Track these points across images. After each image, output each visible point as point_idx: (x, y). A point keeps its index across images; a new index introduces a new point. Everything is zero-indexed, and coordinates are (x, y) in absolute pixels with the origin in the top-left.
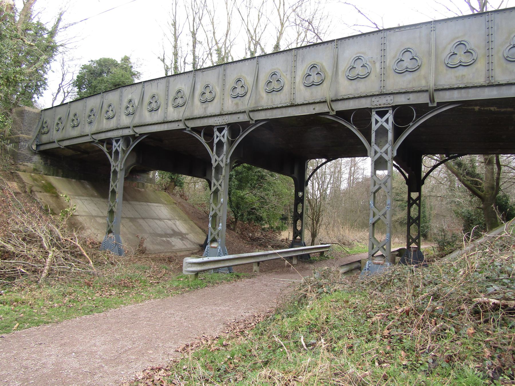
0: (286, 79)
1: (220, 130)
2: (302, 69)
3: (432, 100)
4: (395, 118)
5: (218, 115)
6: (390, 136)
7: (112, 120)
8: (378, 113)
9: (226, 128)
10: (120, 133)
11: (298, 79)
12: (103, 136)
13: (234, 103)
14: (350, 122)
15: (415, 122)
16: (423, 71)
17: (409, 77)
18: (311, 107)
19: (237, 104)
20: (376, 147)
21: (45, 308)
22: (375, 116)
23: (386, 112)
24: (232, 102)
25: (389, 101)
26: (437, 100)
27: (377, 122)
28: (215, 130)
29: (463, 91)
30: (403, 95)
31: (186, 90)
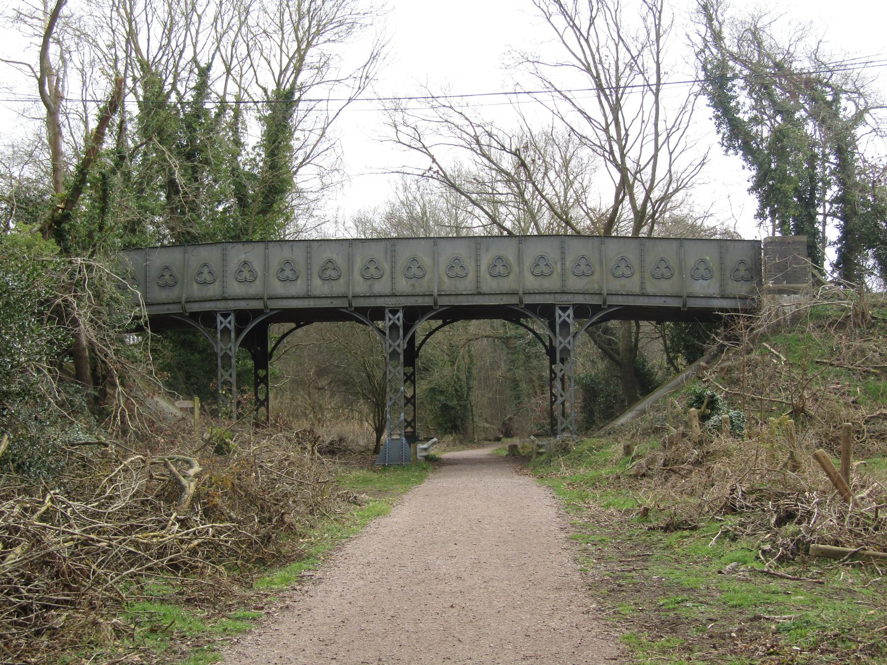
0: (471, 266)
1: (394, 312)
2: (486, 261)
3: (605, 302)
4: (404, 316)
5: (303, 298)
6: (233, 335)
7: (211, 286)
8: (222, 315)
9: (401, 311)
10: (232, 305)
11: (483, 268)
12: (195, 308)
13: (409, 283)
14: (536, 313)
15: (591, 318)
16: (596, 277)
17: (585, 280)
18: (499, 297)
19: (413, 285)
20: (560, 339)
21: (690, 642)
22: (220, 318)
23: (397, 311)
24: (407, 282)
25: (570, 299)
26: (439, 304)
27: (560, 316)
28: (387, 311)
29: (625, 297)
30: (581, 295)
31: (511, 257)
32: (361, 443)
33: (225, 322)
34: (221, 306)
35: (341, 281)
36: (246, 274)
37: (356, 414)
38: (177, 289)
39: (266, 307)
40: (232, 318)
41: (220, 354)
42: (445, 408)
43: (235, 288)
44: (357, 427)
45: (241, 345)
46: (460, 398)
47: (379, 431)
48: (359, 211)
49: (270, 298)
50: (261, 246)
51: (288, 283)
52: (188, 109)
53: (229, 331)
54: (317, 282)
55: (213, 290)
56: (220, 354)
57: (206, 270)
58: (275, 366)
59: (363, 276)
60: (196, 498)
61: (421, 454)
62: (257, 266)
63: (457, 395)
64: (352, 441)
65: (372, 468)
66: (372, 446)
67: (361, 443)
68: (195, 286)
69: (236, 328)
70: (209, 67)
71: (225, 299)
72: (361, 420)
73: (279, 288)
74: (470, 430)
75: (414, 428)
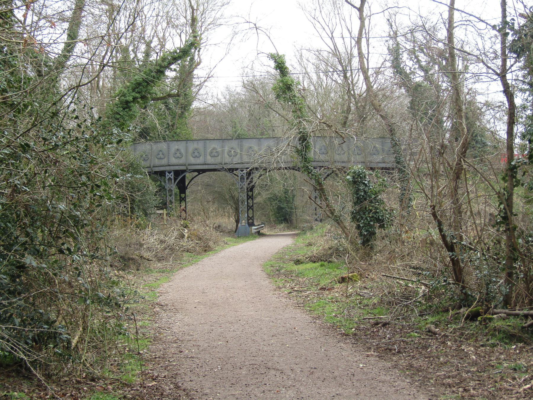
6: (173, 181)
12: (157, 169)
22: (167, 174)
32: (229, 228)
33: (170, 175)
34: (168, 168)
35: (219, 157)
36: (178, 155)
37: (227, 214)
38: (148, 162)
39: (187, 169)
40: (172, 173)
41: (168, 189)
42: (280, 209)
43: (173, 161)
44: (227, 220)
45: (177, 185)
46: (288, 202)
47: (237, 221)
48: (228, 88)
49: (189, 165)
50: (185, 142)
51: (196, 159)
52: (141, 63)
53: (171, 179)
54: (209, 157)
55: (164, 162)
56: (168, 189)
57: (161, 153)
58: (187, 191)
59: (228, 155)
60: (188, 238)
61: (254, 231)
62: (183, 151)
63: (286, 200)
64: (225, 227)
65: (233, 237)
66: (234, 230)
67: (229, 228)
68: (156, 160)
69: (174, 178)
70: (151, 42)
71: (169, 165)
72: (229, 217)
73: (192, 160)
74: (294, 221)
75: (253, 220)
